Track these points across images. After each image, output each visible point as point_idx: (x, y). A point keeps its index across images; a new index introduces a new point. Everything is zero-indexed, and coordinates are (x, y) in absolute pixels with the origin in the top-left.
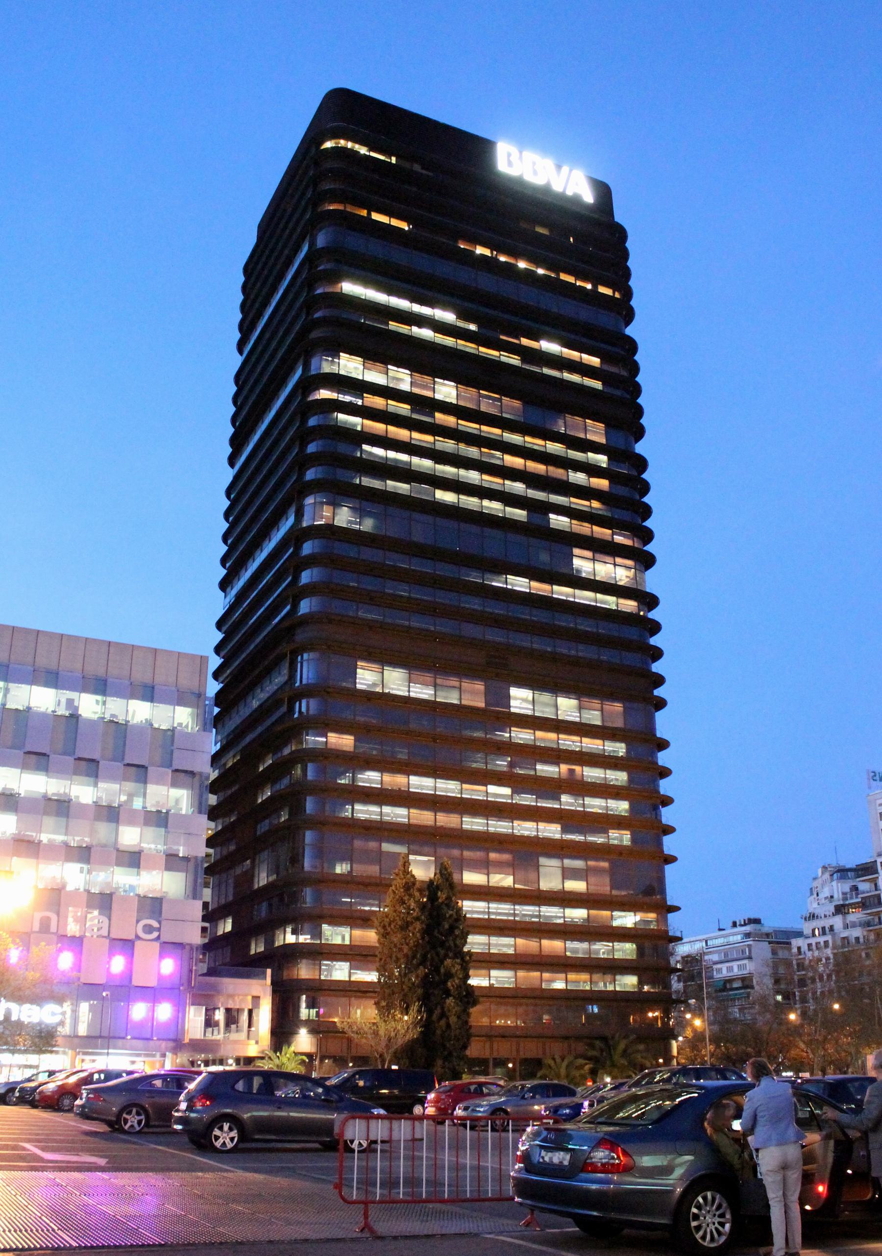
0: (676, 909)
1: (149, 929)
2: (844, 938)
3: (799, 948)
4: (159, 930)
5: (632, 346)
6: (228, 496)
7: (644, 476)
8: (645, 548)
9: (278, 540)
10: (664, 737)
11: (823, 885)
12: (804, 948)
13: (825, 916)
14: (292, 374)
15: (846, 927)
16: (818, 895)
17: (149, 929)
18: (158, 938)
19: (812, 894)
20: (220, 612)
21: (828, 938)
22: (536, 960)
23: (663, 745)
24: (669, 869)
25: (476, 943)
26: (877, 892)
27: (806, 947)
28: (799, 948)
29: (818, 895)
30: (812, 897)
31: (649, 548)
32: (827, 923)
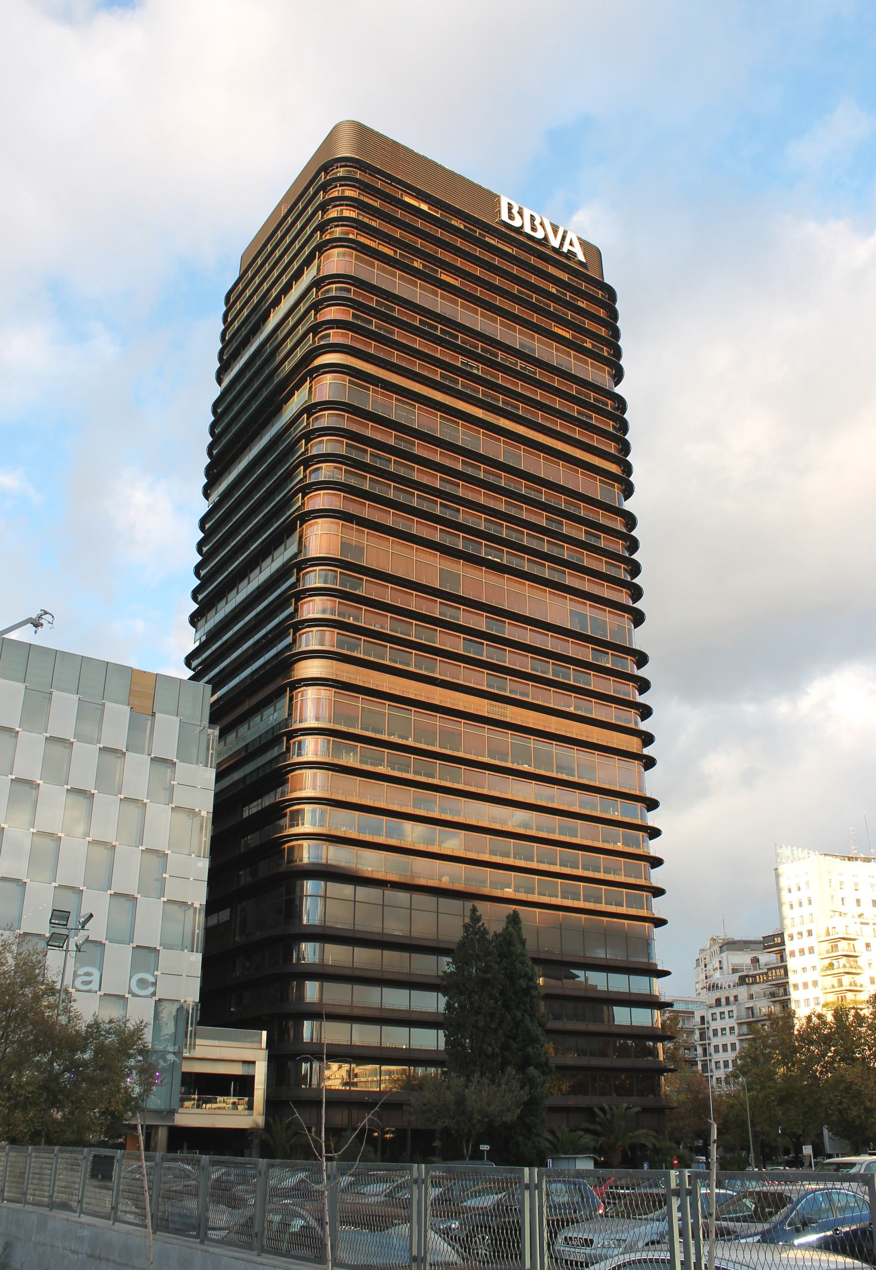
0: (666, 973)
1: (142, 983)
2: (748, 1008)
3: (703, 1018)
4: (154, 984)
5: (621, 404)
6: (200, 551)
7: (633, 533)
8: (635, 605)
9: (227, 612)
10: (656, 826)
11: (712, 955)
12: (708, 1018)
13: (729, 987)
14: (227, 473)
15: (751, 997)
16: (706, 966)
17: (142, 983)
18: (154, 994)
19: (698, 965)
20: (192, 646)
21: (733, 1008)
22: (376, 1014)
23: (652, 804)
24: (657, 932)
25: (432, 1003)
26: (783, 964)
27: (710, 1018)
28: (703, 1018)
29: (706, 966)
30: (699, 968)
31: (638, 605)
32: (731, 994)
